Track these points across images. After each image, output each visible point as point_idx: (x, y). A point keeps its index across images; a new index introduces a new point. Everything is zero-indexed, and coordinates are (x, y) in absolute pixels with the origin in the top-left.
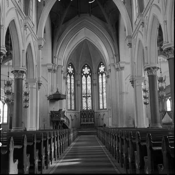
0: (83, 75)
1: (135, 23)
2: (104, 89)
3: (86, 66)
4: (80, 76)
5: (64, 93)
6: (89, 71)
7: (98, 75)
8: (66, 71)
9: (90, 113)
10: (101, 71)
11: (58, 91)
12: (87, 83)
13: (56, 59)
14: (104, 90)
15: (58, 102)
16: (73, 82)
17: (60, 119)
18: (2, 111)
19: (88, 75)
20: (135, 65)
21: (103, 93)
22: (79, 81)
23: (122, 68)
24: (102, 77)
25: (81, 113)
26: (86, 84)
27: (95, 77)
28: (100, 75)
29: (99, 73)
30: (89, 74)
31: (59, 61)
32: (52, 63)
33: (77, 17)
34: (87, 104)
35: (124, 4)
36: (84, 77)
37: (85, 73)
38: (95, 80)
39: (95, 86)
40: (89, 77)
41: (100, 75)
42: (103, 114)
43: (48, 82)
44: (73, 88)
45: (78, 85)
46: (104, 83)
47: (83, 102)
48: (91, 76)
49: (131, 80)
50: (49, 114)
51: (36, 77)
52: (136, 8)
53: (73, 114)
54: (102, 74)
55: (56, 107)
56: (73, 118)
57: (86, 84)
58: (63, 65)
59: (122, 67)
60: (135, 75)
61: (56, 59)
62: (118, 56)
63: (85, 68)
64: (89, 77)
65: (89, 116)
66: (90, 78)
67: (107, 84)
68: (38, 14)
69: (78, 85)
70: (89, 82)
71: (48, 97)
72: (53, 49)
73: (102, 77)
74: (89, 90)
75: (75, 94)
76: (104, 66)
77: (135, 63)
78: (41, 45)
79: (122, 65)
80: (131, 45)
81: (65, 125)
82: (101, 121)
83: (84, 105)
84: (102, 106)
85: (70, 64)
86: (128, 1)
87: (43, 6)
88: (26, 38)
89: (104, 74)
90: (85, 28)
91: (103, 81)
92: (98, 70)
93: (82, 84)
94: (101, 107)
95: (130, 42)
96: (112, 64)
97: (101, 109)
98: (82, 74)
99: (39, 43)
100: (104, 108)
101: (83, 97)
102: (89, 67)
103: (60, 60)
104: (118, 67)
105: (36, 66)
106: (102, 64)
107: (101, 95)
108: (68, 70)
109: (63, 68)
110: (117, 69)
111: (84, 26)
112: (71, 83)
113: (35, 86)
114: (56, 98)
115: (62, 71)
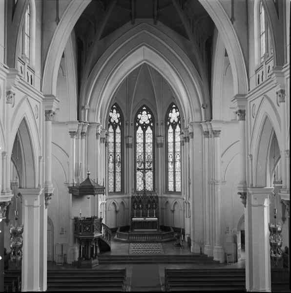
0: (138, 126)
1: (257, 71)
2: (178, 156)
3: (144, 108)
4: (132, 128)
5: (101, 183)
6: (149, 119)
7: (167, 128)
8: (107, 119)
9: (149, 201)
10: (172, 121)
11: (88, 179)
12: (146, 141)
13: (87, 111)
14: (178, 158)
15: (88, 199)
16: (118, 140)
17: (93, 235)
18: (2, 121)
19: (147, 125)
20: (252, 160)
21: (174, 162)
22: (129, 138)
23: (216, 133)
24: (174, 132)
25: (134, 200)
26: (144, 143)
27: (161, 131)
28: (170, 127)
29: (168, 123)
30: (149, 125)
31: (92, 115)
32: (78, 120)
33: (128, 25)
34: (144, 182)
35: (233, 23)
36: (140, 131)
37: (141, 122)
38: (160, 138)
39: (160, 149)
40: (149, 130)
41: (170, 127)
42: (175, 202)
43: (71, 156)
44: (118, 150)
45: (128, 146)
46: (178, 144)
47: (137, 177)
48: (152, 128)
49: (242, 191)
50: (71, 221)
51: (41, 184)
52: (260, 36)
53: (118, 201)
54: (174, 125)
55: (83, 209)
56: (118, 208)
57: (144, 143)
58: (99, 122)
59: (215, 131)
60: (250, 183)
61: (87, 111)
62: (208, 110)
63: (119, 120)
64: (149, 130)
65: (147, 205)
66: (151, 132)
67: (182, 147)
68: (45, 42)
69: (128, 144)
70: (149, 140)
71: (69, 187)
72: (82, 81)
73: (174, 132)
74: (148, 154)
75: (122, 162)
76: (178, 111)
77: (251, 156)
78: (50, 111)
79: (215, 127)
80: (245, 115)
81: (103, 241)
82: (170, 213)
83: (140, 182)
84: (173, 185)
85: (114, 106)
86: (241, 17)
87: (55, 23)
88: (10, 120)
89: (178, 126)
90: (144, 47)
91: (176, 140)
92: (167, 119)
93: (135, 143)
94: (171, 188)
95: (242, 109)
96: (196, 122)
97: (171, 193)
98: (137, 124)
99: (46, 107)
100: (177, 191)
101: (138, 169)
102: (149, 111)
103: (94, 111)
104: (208, 129)
105: (40, 158)
106: (174, 106)
107: (170, 166)
108: (111, 117)
109: (99, 129)
110: (206, 134)
111: (143, 43)
112: (115, 143)
113: (37, 203)
114: (84, 190)
115: (97, 134)
